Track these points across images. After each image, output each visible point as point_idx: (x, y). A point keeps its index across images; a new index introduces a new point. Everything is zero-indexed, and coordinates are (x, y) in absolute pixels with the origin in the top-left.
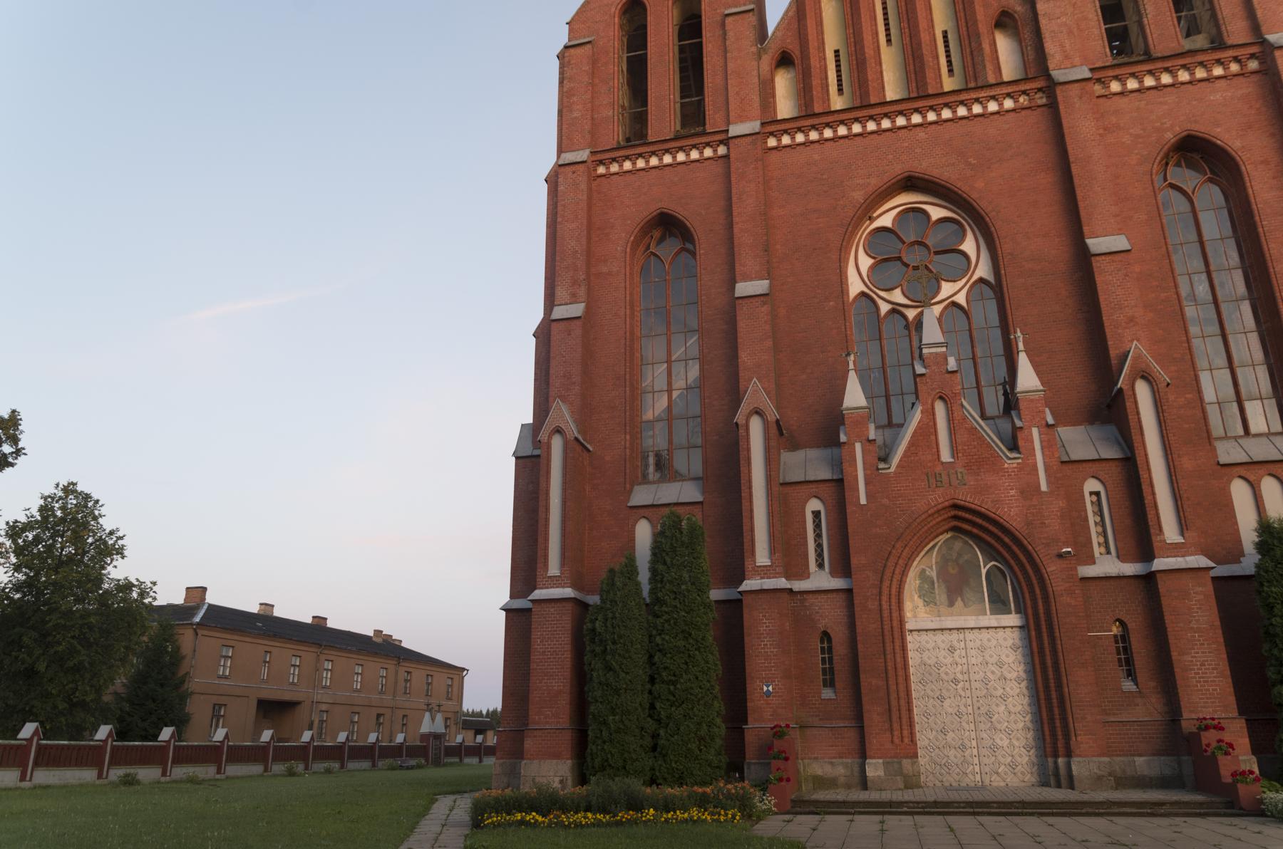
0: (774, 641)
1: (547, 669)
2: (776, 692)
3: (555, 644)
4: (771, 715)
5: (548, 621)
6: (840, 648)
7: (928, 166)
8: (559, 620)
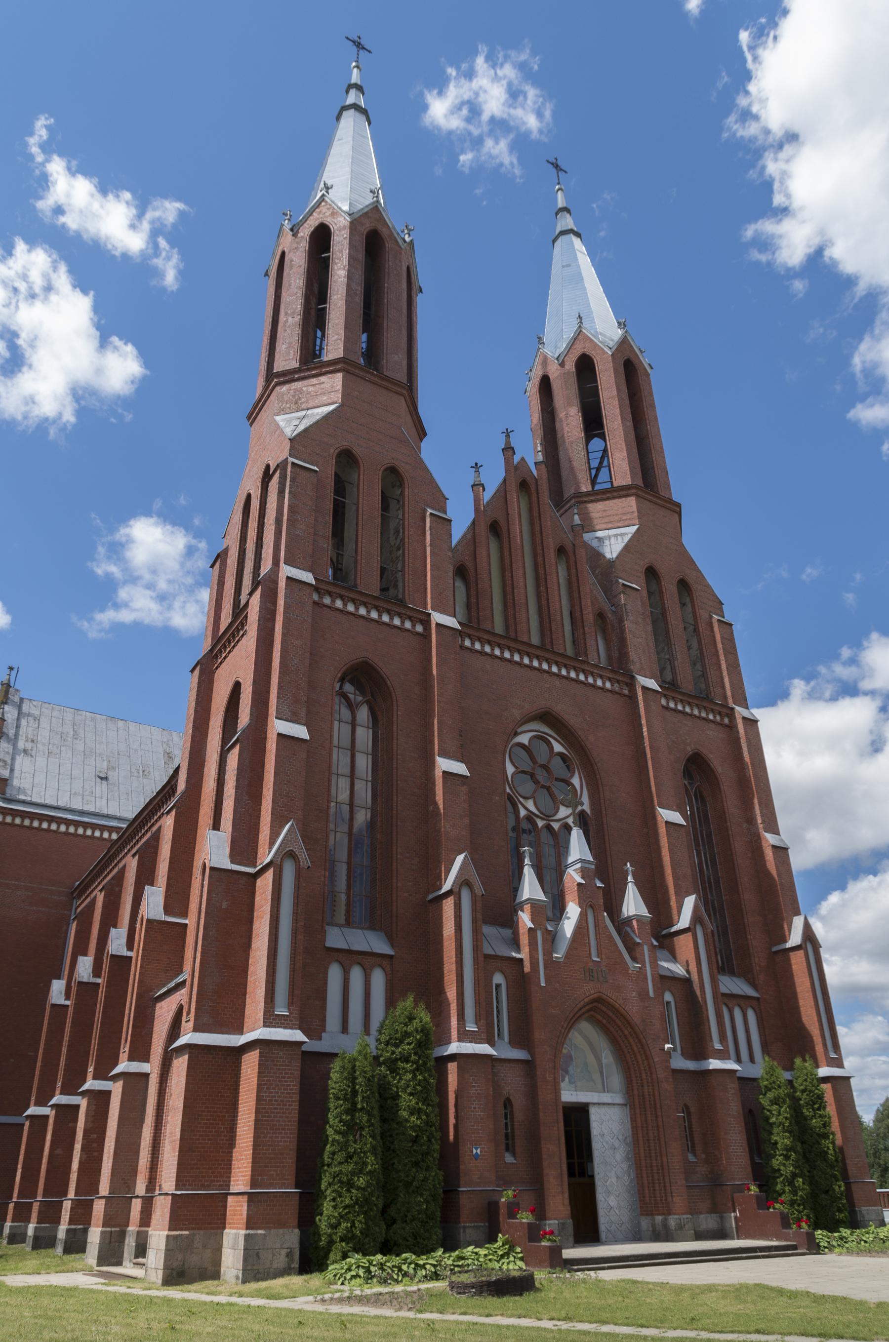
0: (481, 1104)
1: (273, 1121)
2: (483, 1155)
3: (283, 1093)
4: (479, 1178)
5: (276, 1065)
6: (519, 1115)
7: (564, 709)
8: (288, 1066)
